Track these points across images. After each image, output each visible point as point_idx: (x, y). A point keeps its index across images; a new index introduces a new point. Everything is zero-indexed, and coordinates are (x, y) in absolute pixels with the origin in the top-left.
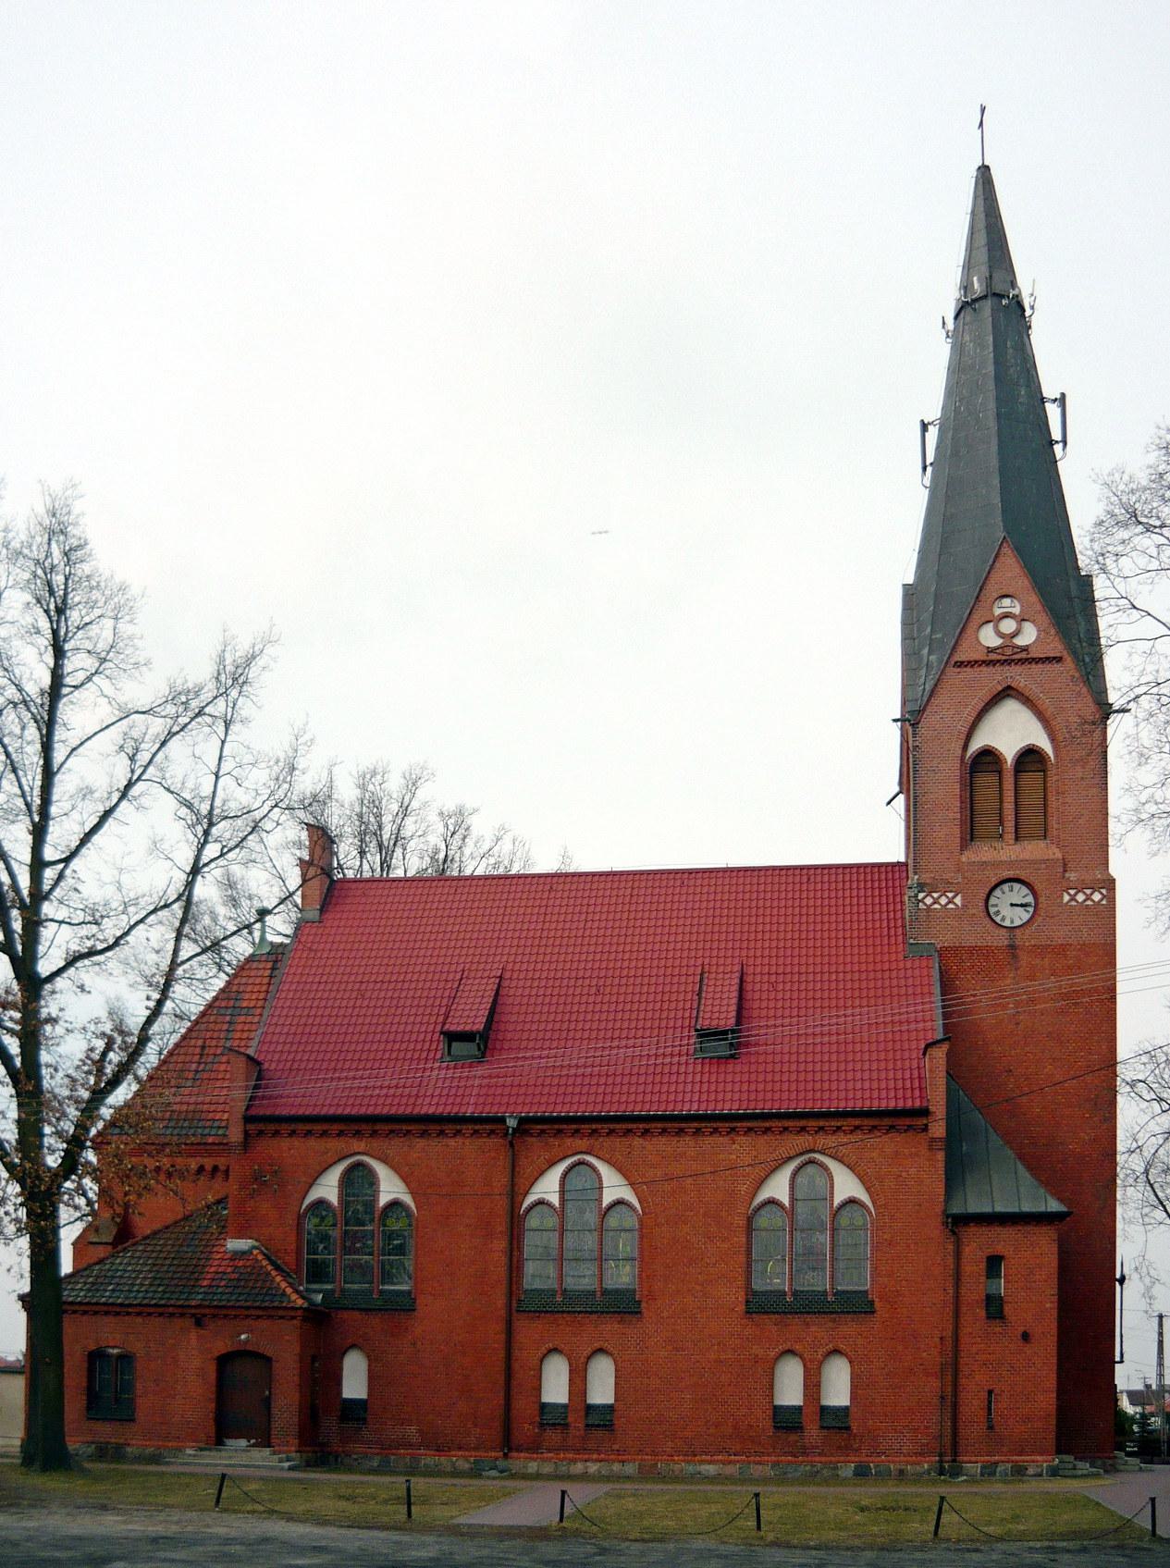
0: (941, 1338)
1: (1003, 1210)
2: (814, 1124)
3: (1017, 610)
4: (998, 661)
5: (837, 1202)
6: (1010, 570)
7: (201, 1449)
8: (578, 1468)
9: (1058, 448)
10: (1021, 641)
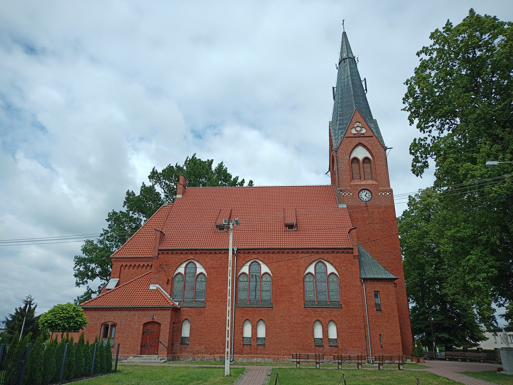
0: (363, 317)
1: (385, 277)
2: (326, 251)
3: (360, 125)
4: (357, 137)
5: (328, 274)
6: (358, 116)
7: (135, 357)
8: (255, 360)
9: (365, 91)
10: (362, 132)
